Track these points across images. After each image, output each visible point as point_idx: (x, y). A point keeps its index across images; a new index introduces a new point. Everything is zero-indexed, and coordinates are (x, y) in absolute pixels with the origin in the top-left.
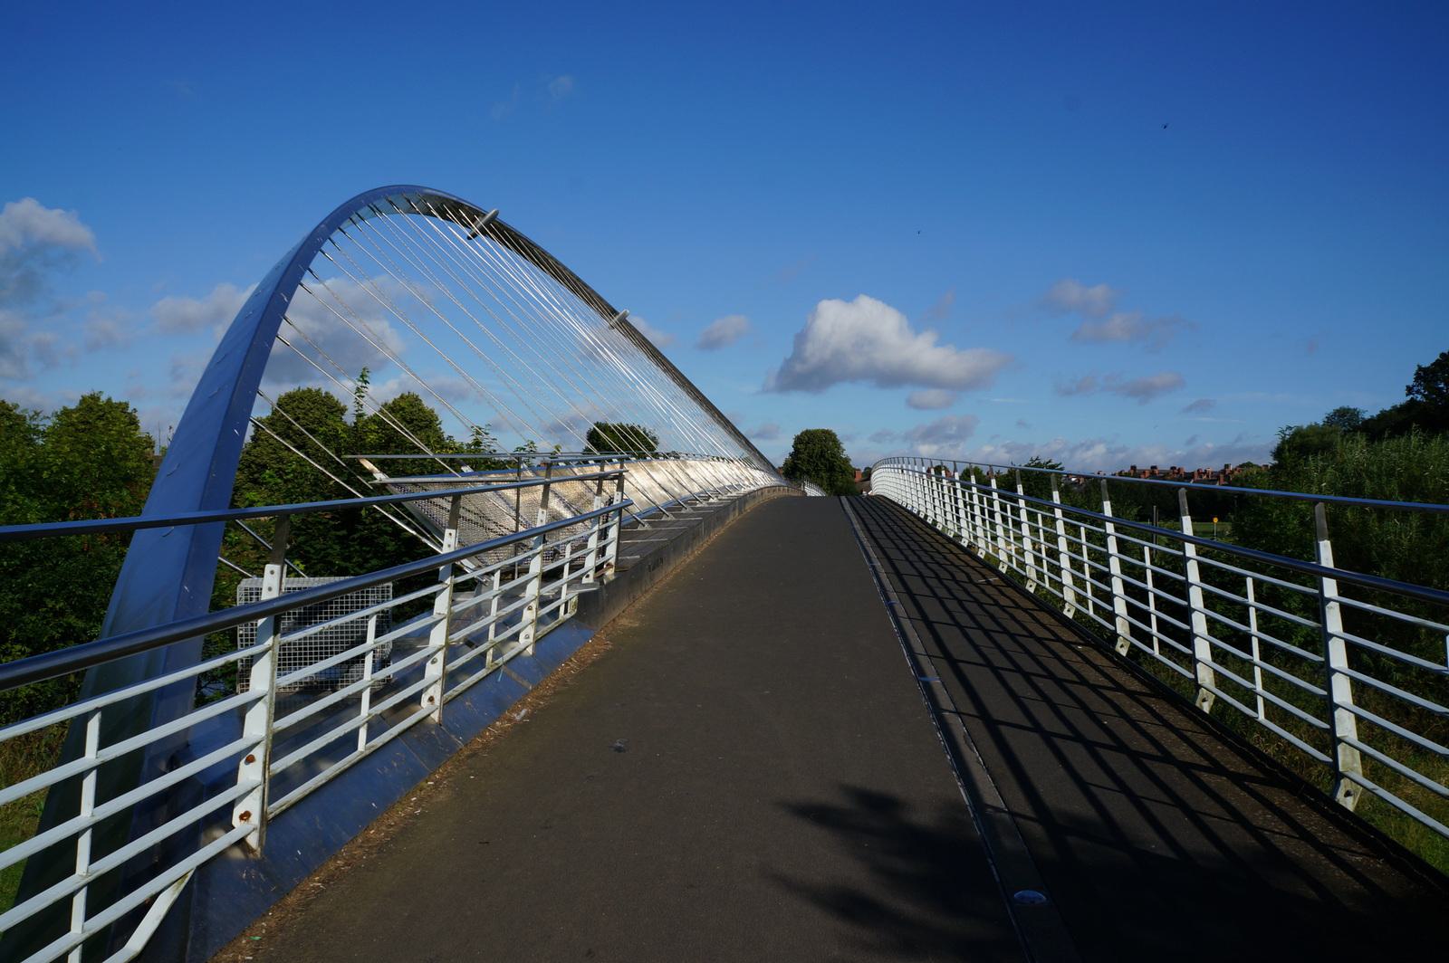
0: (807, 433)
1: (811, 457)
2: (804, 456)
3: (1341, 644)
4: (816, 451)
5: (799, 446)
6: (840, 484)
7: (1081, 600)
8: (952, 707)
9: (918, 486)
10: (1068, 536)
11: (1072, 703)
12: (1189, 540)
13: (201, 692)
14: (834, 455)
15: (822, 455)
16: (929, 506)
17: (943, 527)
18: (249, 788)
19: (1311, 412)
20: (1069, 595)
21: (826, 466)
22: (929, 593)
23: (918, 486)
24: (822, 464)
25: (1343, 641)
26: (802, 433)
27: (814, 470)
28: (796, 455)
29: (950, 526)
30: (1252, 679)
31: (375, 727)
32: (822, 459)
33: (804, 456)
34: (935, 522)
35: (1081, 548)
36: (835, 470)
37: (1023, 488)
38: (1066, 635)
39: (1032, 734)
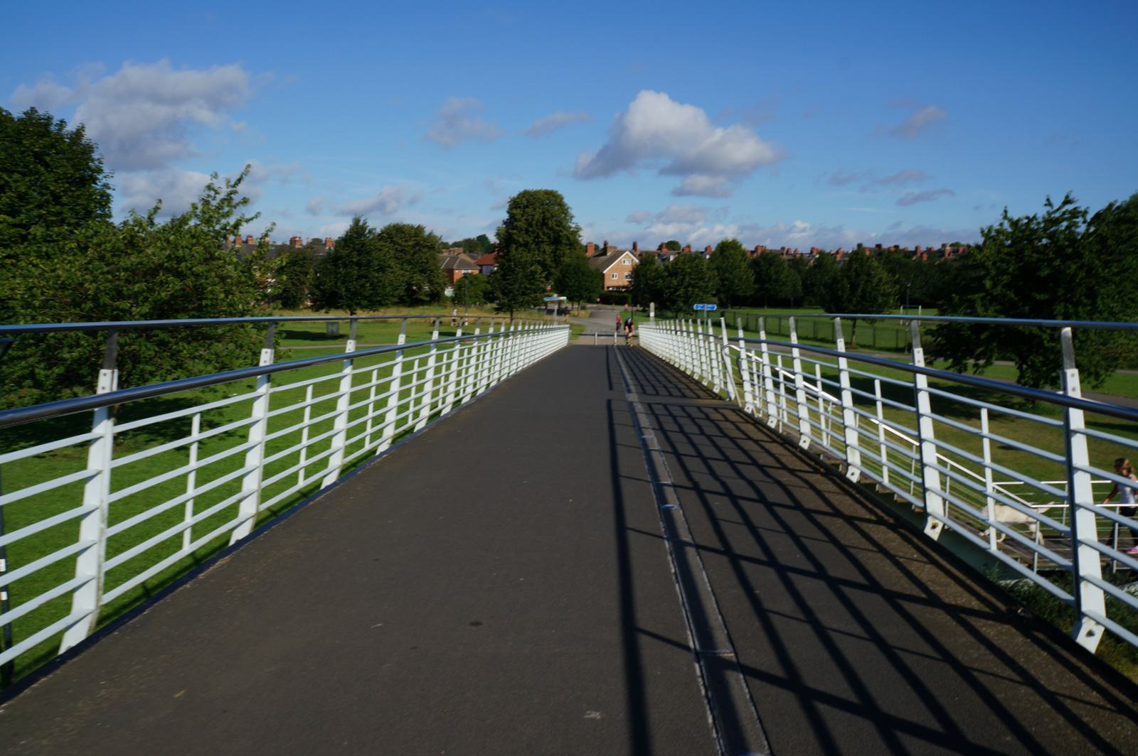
0: (525, 194)
1: (530, 225)
2: (522, 224)
3: (1091, 518)
4: (536, 217)
5: (515, 211)
6: (566, 260)
7: (816, 430)
8: (765, 659)
9: (694, 347)
10: (1106, 549)
11: (820, 535)
12: (921, 371)
13: (51, 466)
14: (560, 224)
15: (544, 223)
16: (696, 363)
17: (709, 382)
18: (83, 615)
19: (1029, 205)
20: (805, 427)
21: (549, 237)
22: (694, 453)
23: (694, 347)
24: (544, 234)
25: (930, 420)
26: (519, 195)
27: (534, 241)
28: (510, 223)
29: (716, 381)
30: (879, 454)
31: (197, 531)
32: (545, 228)
33: (522, 224)
34: (693, 373)
35: (814, 368)
36: (561, 243)
37: (925, 353)
38: (846, 504)
39: (756, 504)
